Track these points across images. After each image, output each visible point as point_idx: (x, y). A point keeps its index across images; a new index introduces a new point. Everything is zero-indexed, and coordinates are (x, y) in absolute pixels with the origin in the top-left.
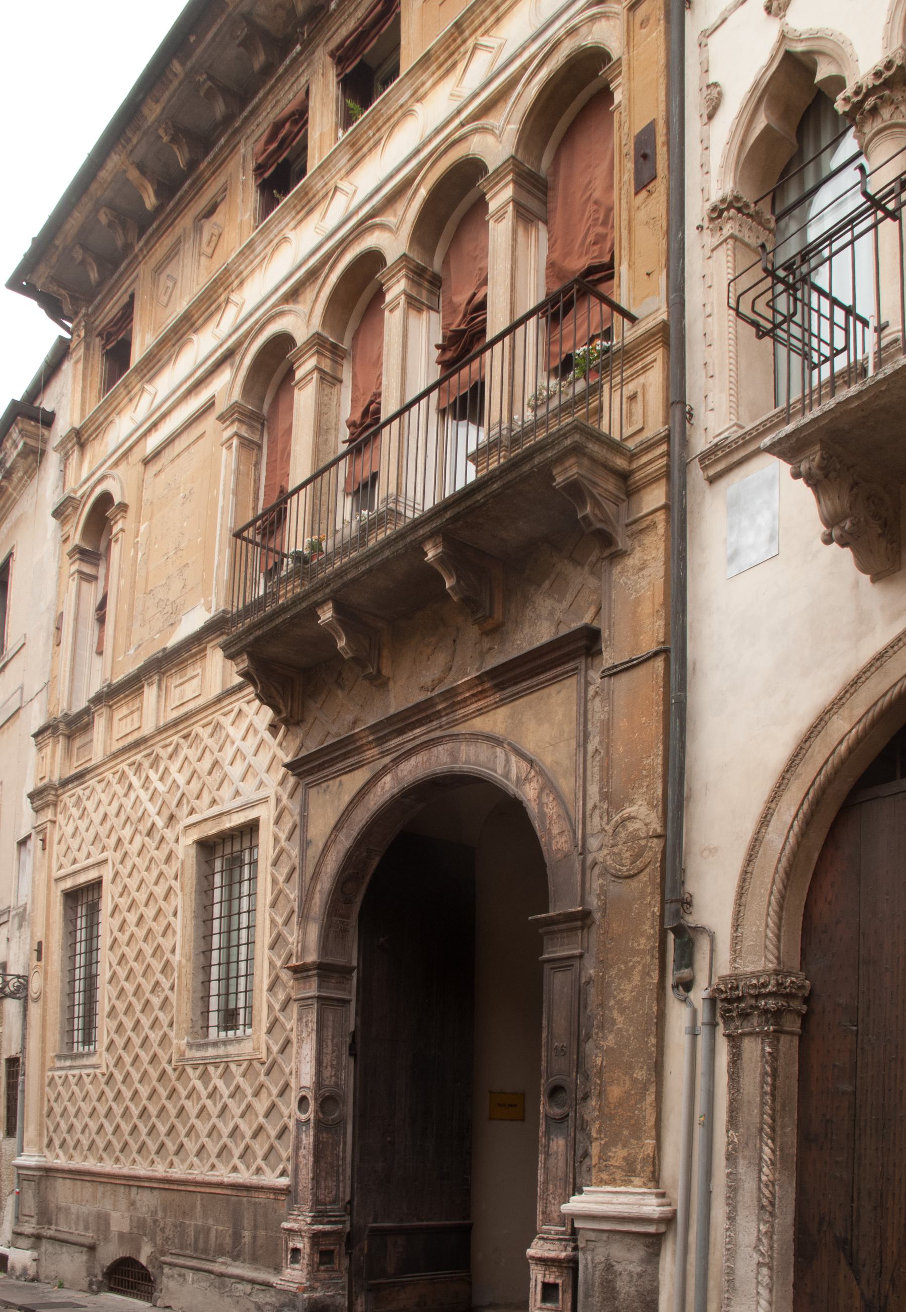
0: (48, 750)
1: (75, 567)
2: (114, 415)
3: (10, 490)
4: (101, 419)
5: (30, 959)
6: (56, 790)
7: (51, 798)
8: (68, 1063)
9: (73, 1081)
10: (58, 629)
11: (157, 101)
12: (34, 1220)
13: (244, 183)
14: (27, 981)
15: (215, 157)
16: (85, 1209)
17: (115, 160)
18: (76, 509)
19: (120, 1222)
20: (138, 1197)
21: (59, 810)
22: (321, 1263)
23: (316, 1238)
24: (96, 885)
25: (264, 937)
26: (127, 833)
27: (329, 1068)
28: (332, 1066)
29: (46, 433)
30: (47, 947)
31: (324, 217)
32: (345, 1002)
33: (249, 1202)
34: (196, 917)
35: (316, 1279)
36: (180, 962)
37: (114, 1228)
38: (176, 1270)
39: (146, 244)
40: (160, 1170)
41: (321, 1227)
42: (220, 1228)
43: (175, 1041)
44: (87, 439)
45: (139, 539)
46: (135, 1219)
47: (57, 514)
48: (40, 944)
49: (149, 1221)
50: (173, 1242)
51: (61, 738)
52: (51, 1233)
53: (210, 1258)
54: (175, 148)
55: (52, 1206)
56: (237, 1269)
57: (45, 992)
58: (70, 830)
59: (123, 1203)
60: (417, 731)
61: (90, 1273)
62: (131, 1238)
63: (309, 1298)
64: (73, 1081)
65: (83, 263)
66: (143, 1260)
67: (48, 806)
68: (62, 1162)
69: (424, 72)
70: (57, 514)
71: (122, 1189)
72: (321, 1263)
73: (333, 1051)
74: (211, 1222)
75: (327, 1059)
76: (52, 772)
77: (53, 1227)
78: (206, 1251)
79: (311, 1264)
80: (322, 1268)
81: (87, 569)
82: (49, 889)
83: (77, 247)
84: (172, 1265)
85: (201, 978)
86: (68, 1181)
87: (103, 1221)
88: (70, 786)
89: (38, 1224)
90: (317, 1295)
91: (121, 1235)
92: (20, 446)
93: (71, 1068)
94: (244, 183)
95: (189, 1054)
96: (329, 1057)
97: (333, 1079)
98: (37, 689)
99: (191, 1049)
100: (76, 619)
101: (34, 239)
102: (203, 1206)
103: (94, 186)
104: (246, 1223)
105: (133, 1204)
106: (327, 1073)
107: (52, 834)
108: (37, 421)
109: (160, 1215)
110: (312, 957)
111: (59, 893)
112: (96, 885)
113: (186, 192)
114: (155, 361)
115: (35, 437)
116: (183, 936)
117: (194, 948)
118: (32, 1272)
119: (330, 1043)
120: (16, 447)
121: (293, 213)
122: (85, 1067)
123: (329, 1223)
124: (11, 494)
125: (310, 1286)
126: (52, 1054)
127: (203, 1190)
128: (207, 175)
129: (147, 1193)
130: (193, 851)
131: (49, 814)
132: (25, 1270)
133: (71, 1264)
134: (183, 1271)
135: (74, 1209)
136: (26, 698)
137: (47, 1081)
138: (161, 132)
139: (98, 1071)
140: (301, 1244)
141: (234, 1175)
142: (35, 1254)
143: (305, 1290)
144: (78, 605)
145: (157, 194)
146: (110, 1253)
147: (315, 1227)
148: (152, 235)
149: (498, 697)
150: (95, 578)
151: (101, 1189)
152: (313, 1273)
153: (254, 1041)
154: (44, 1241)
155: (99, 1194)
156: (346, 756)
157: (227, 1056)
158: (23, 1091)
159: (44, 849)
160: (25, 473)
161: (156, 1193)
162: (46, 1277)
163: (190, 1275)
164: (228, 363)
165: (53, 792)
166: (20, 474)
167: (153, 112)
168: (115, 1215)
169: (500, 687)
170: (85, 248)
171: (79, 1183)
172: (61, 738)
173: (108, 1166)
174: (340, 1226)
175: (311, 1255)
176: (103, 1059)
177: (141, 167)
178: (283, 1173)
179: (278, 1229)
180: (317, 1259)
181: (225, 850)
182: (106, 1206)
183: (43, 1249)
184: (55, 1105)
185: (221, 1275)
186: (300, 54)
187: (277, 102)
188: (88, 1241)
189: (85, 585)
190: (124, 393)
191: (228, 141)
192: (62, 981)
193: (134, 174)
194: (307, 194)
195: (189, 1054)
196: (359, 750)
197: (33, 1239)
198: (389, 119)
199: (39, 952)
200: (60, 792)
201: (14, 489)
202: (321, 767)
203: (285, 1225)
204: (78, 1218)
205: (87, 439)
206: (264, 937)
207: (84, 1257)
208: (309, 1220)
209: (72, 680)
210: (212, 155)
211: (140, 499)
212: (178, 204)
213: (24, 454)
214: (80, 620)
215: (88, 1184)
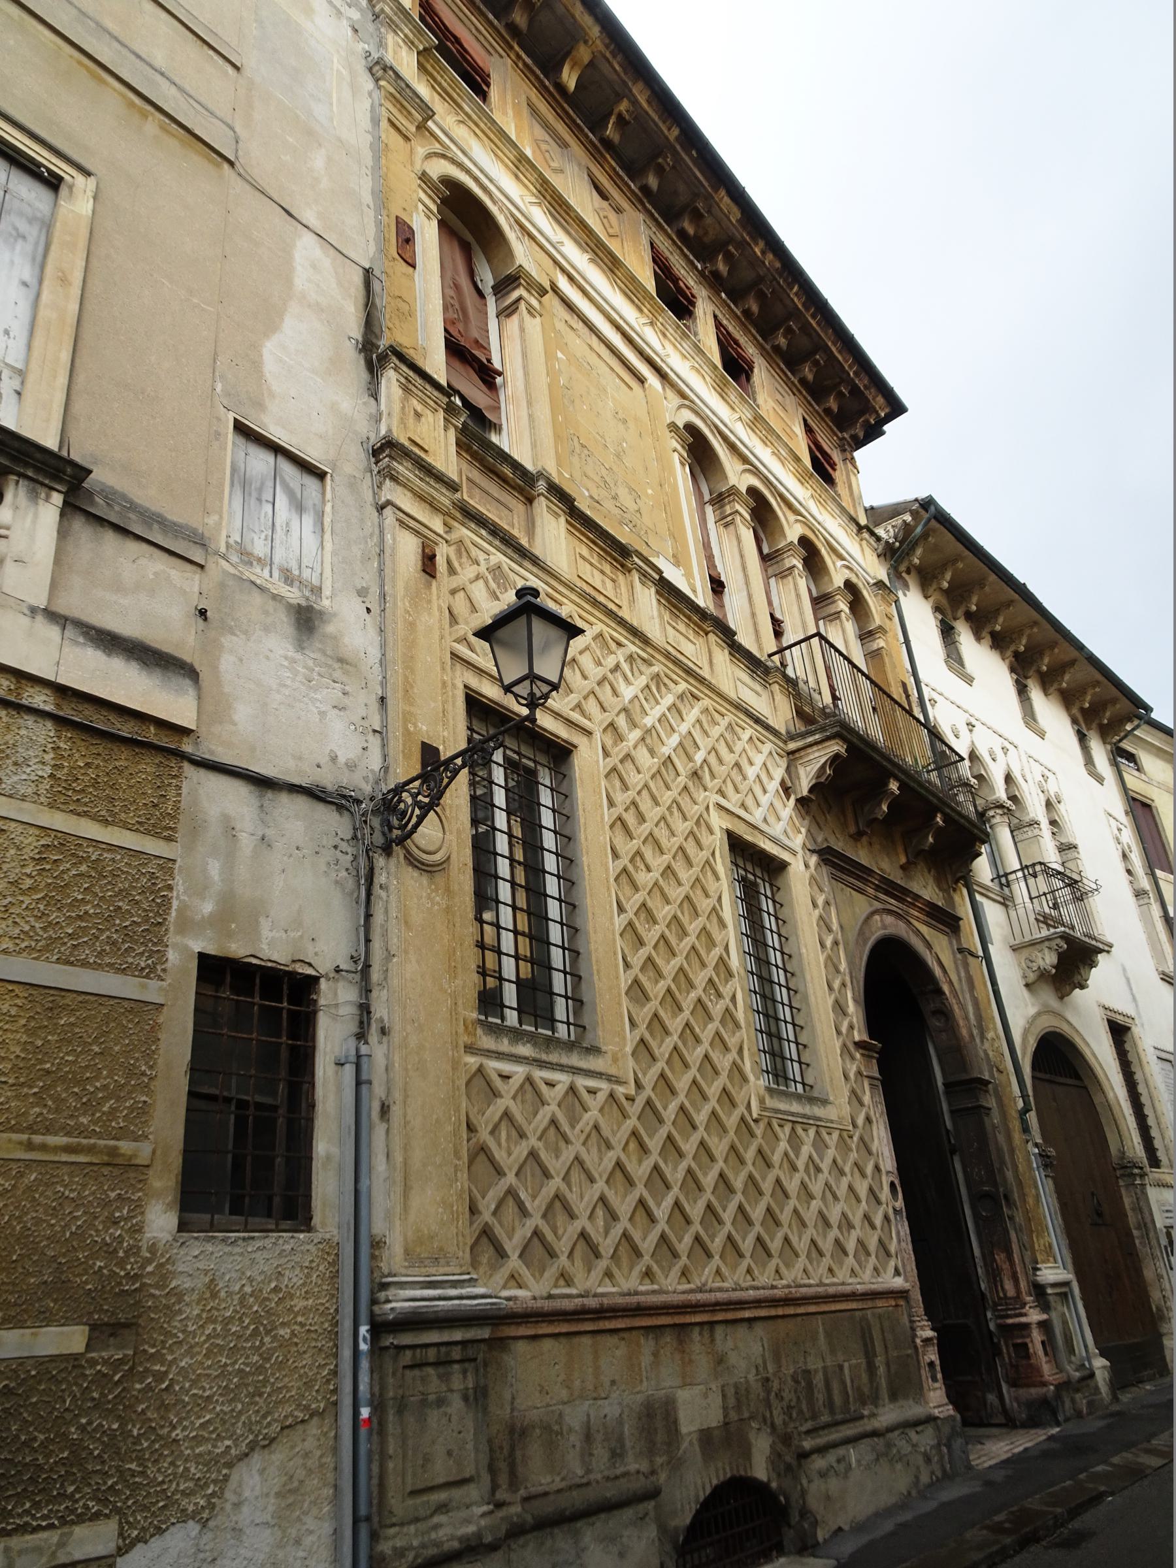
16: (611, 1409)
19: (698, 1409)
20: (730, 1343)
25: (400, 612)
33: (873, 1315)
37: (689, 1424)
38: (831, 1457)
42: (854, 1361)
46: (731, 1392)
49: (756, 1387)
50: (801, 1412)
59: (702, 1363)
60: (893, 901)
62: (725, 1438)
66: (760, 1471)
74: (841, 1358)
84: (821, 1450)
86: (547, 1344)
87: (658, 1419)
91: (706, 1437)
99: (772, 1097)
102: (828, 1335)
105: (720, 1360)
113: (587, 137)
122: (562, 1068)
129: (742, 1331)
134: (841, 1451)
135: (575, 1417)
146: (690, 1487)
149: (925, 918)
155: (646, 1359)
156: (858, 878)
161: (759, 1329)
163: (852, 1454)
169: (928, 914)
171: (586, 1340)
186: (696, 268)
196: (865, 881)
202: (842, 869)
204: (588, 1437)
206: (400, 612)
212: (578, 126)
215: (612, 1340)
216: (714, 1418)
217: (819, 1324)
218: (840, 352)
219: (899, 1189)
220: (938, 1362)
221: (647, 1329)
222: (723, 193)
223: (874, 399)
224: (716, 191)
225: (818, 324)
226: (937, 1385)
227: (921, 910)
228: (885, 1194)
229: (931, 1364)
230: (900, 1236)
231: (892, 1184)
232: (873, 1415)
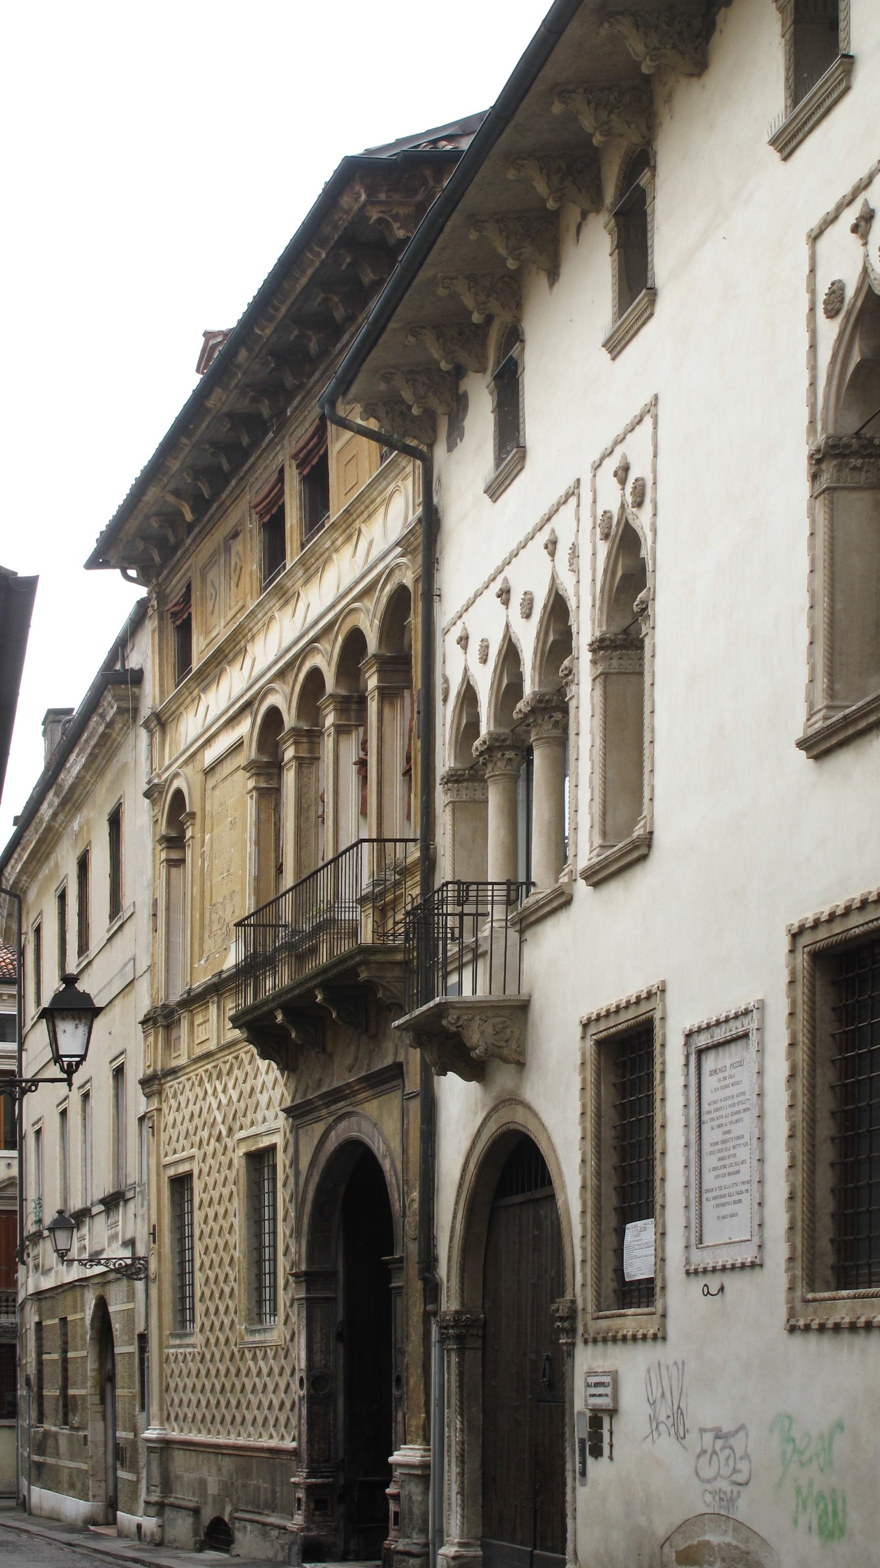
0: (151, 1039)
1: (163, 856)
2: (182, 708)
3: (114, 735)
4: (174, 708)
5: (149, 1242)
6: (160, 1079)
7: (155, 1088)
8: (177, 1342)
9: (180, 1358)
10: (155, 915)
11: (176, 458)
12: (158, 1490)
13: (251, 531)
14: (147, 1262)
15: (231, 492)
17: (153, 492)
18: (161, 793)
21: (163, 1098)
22: (316, 1509)
23: (310, 1489)
24: (189, 1176)
26: (205, 1134)
27: (319, 1354)
28: (321, 1352)
29: (136, 690)
30: (160, 1230)
31: (294, 615)
32: (333, 1300)
34: (248, 1219)
35: (312, 1522)
36: (239, 1258)
39: (194, 540)
40: (232, 1440)
41: (314, 1480)
43: (238, 1327)
44: (167, 719)
45: (205, 848)
47: (147, 795)
48: (154, 1226)
51: (160, 1029)
52: (172, 1500)
53: (260, 1511)
54: (199, 484)
55: (172, 1475)
56: (271, 1520)
57: (160, 1274)
58: (170, 1120)
59: (214, 1470)
61: (196, 1533)
63: (305, 1536)
64: (180, 1358)
65: (145, 549)
67: (154, 1094)
68: (175, 1435)
69: (335, 532)
70: (147, 795)
71: (213, 1457)
72: (316, 1509)
73: (322, 1340)
75: (316, 1347)
76: (155, 1061)
77: (173, 1495)
78: (258, 1506)
79: (308, 1510)
80: (317, 1513)
81: (175, 855)
82: (158, 1175)
83: (138, 539)
85: (255, 1271)
88: (169, 1078)
89: (161, 1493)
90: (313, 1533)
91: (214, 1497)
92: (115, 708)
93: (179, 1346)
94: (251, 531)
95: (248, 1338)
96: (318, 1345)
97: (323, 1362)
98: (144, 970)
100: (168, 909)
101: (97, 540)
103: (141, 505)
104: (278, 1483)
106: (317, 1357)
107: (159, 1122)
108: (126, 683)
109: (235, 1477)
110: (303, 1267)
111: (166, 1179)
112: (189, 1176)
114: (205, 675)
115: (124, 698)
116: (240, 1236)
117: (248, 1246)
118: (157, 1538)
119: (318, 1333)
120: (112, 707)
121: (277, 598)
123: (321, 1477)
124: (115, 739)
125: (307, 1527)
126: (168, 1332)
127: (258, 1454)
128: (228, 503)
130: (243, 1162)
131: (155, 1104)
132: (152, 1534)
133: (182, 1528)
136: (138, 974)
137: (164, 1357)
138: (184, 475)
139: (196, 1350)
140: (301, 1494)
141: (270, 1441)
142: (160, 1522)
143: (302, 1530)
144: (168, 893)
145: (193, 510)
146: (208, 1514)
147: (308, 1481)
148: (197, 535)
150: (183, 861)
151: (201, 1457)
152: (309, 1518)
153: (276, 1332)
154: (166, 1508)
157: (265, 1342)
158: (148, 1367)
159: (153, 1136)
160: (124, 725)
162: (169, 1542)
163: (249, 1527)
164: (248, 712)
165: (157, 1082)
166: (120, 725)
167: (175, 465)
168: (210, 1480)
169: (372, 1086)
170: (145, 539)
172: (160, 1029)
173: (202, 1438)
174: (331, 1480)
175: (307, 1503)
176: (198, 1339)
177: (176, 493)
178: (294, 1440)
179: (288, 1482)
180: (312, 1506)
181: (260, 1160)
182: (204, 1473)
183: (166, 1516)
184: (170, 1380)
185: (264, 1524)
187: (266, 467)
188: (191, 1505)
189: (174, 871)
190: (187, 693)
191: (237, 484)
192: (173, 1263)
193: (171, 499)
194: (282, 588)
195: (248, 1338)
196: (317, 1109)
197: (157, 1507)
198: (322, 555)
199: (154, 1234)
200: (163, 1081)
201: (118, 735)
203: (293, 1480)
205: (167, 719)
207: (190, 1520)
208: (304, 1475)
209: (167, 971)
210: (229, 488)
211: (203, 808)
213: (121, 711)
214: (172, 907)
216: (216, 1493)
217: (254, 1460)
218: (304, 272)
219: (305, 1381)
220: (304, 1499)
221: (194, 1451)
222: (210, 403)
223: (347, 212)
224: (209, 410)
225: (282, 302)
226: (300, 1512)
227: (364, 1089)
228: (295, 1386)
229: (299, 1499)
230: (298, 1418)
231: (301, 1380)
232: (267, 1515)
